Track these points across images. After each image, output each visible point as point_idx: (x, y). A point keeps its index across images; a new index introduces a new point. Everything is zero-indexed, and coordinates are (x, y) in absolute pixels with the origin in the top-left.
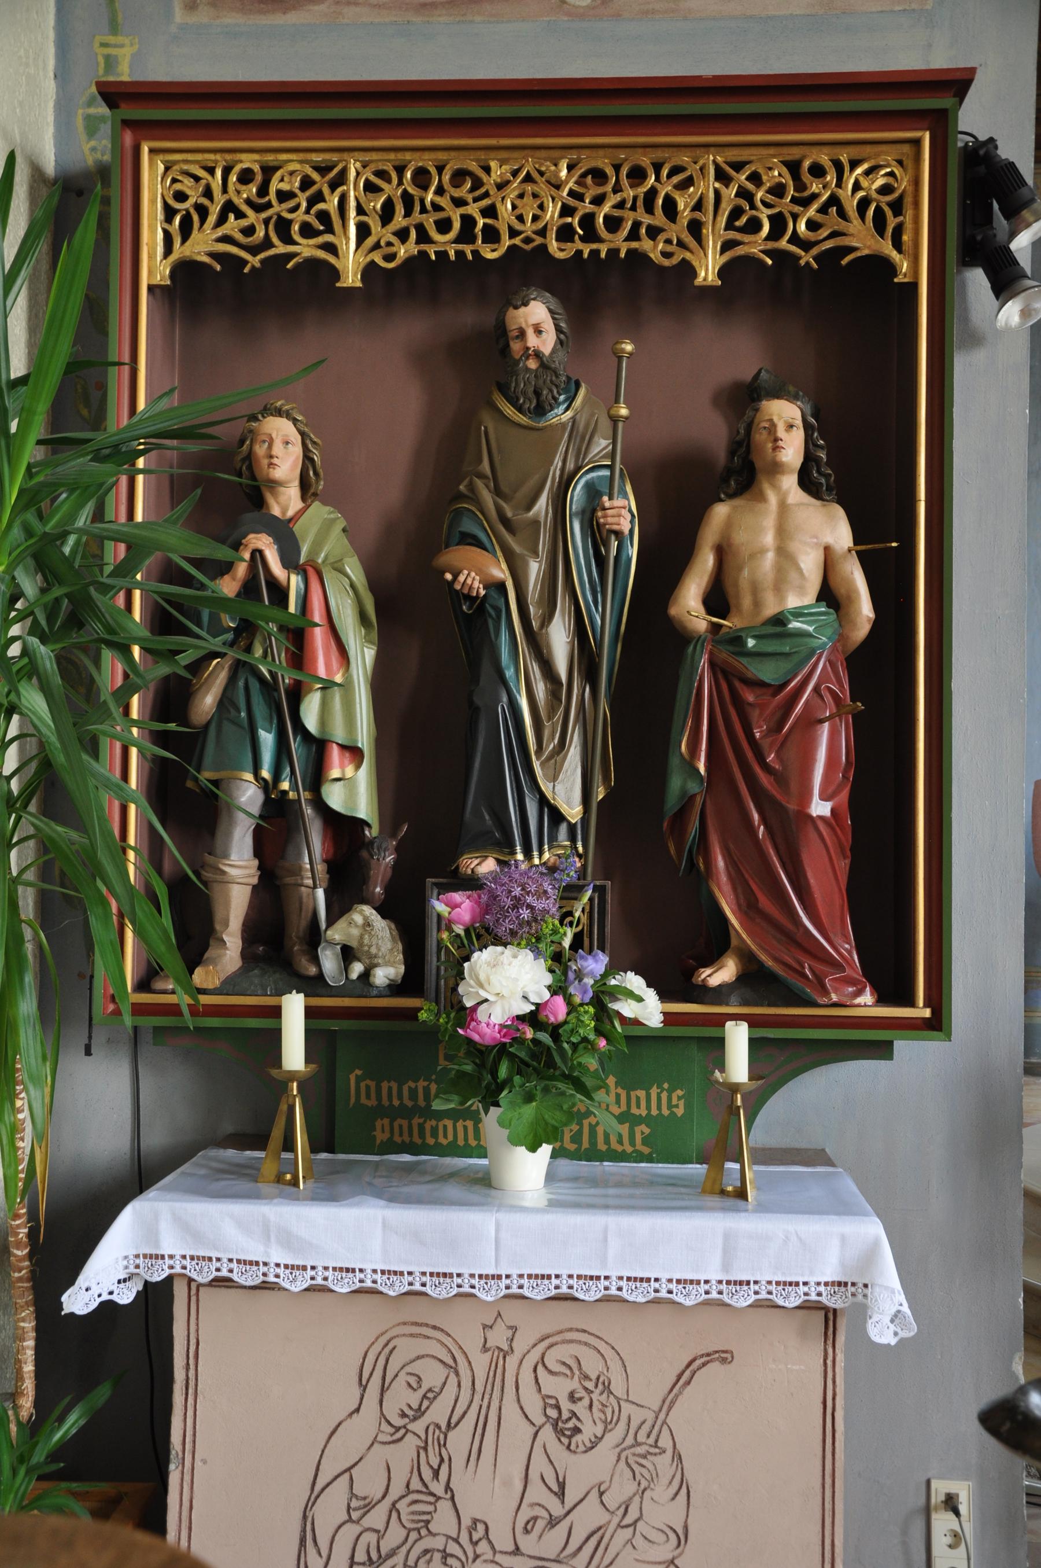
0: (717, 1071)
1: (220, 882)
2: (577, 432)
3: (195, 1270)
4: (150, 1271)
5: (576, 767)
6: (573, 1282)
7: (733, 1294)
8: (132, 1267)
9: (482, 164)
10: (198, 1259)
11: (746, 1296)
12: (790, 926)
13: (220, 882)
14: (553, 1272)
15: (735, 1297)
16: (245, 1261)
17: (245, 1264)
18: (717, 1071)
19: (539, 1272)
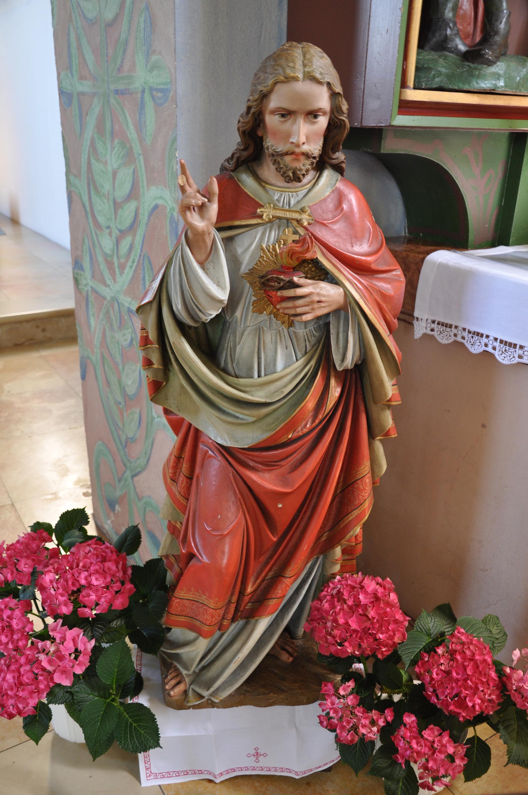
0: (127, 637)
1: (450, 791)
2: (360, 509)
3: (470, 342)
4: (503, 355)
5: (237, 442)
6: (497, 344)
7: (441, 332)
8: (429, 329)
9: (76, 276)
10: (438, 324)
11: (448, 336)
12: (321, 566)
13: (450, 791)
14: (519, 343)
15: (441, 335)
16: (506, 342)
17: (506, 344)
18: (127, 637)
19: (509, 340)
